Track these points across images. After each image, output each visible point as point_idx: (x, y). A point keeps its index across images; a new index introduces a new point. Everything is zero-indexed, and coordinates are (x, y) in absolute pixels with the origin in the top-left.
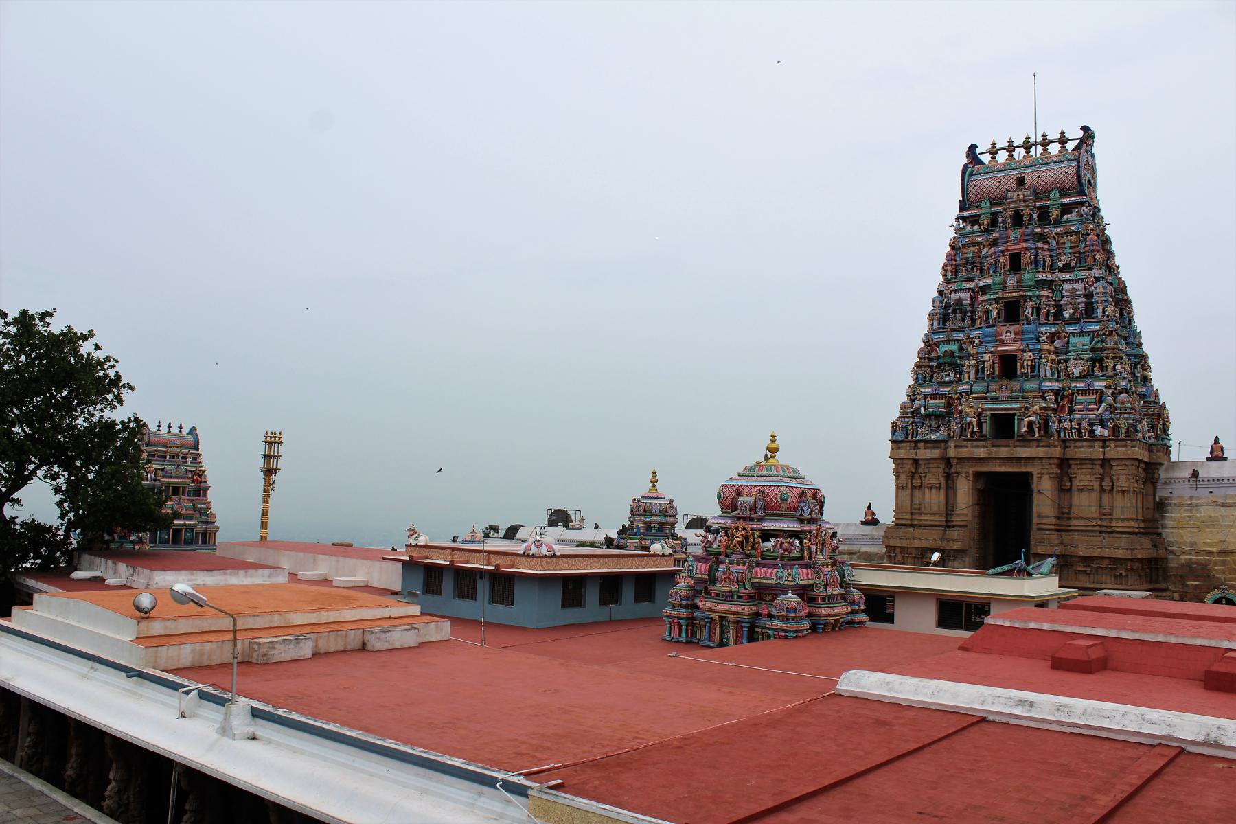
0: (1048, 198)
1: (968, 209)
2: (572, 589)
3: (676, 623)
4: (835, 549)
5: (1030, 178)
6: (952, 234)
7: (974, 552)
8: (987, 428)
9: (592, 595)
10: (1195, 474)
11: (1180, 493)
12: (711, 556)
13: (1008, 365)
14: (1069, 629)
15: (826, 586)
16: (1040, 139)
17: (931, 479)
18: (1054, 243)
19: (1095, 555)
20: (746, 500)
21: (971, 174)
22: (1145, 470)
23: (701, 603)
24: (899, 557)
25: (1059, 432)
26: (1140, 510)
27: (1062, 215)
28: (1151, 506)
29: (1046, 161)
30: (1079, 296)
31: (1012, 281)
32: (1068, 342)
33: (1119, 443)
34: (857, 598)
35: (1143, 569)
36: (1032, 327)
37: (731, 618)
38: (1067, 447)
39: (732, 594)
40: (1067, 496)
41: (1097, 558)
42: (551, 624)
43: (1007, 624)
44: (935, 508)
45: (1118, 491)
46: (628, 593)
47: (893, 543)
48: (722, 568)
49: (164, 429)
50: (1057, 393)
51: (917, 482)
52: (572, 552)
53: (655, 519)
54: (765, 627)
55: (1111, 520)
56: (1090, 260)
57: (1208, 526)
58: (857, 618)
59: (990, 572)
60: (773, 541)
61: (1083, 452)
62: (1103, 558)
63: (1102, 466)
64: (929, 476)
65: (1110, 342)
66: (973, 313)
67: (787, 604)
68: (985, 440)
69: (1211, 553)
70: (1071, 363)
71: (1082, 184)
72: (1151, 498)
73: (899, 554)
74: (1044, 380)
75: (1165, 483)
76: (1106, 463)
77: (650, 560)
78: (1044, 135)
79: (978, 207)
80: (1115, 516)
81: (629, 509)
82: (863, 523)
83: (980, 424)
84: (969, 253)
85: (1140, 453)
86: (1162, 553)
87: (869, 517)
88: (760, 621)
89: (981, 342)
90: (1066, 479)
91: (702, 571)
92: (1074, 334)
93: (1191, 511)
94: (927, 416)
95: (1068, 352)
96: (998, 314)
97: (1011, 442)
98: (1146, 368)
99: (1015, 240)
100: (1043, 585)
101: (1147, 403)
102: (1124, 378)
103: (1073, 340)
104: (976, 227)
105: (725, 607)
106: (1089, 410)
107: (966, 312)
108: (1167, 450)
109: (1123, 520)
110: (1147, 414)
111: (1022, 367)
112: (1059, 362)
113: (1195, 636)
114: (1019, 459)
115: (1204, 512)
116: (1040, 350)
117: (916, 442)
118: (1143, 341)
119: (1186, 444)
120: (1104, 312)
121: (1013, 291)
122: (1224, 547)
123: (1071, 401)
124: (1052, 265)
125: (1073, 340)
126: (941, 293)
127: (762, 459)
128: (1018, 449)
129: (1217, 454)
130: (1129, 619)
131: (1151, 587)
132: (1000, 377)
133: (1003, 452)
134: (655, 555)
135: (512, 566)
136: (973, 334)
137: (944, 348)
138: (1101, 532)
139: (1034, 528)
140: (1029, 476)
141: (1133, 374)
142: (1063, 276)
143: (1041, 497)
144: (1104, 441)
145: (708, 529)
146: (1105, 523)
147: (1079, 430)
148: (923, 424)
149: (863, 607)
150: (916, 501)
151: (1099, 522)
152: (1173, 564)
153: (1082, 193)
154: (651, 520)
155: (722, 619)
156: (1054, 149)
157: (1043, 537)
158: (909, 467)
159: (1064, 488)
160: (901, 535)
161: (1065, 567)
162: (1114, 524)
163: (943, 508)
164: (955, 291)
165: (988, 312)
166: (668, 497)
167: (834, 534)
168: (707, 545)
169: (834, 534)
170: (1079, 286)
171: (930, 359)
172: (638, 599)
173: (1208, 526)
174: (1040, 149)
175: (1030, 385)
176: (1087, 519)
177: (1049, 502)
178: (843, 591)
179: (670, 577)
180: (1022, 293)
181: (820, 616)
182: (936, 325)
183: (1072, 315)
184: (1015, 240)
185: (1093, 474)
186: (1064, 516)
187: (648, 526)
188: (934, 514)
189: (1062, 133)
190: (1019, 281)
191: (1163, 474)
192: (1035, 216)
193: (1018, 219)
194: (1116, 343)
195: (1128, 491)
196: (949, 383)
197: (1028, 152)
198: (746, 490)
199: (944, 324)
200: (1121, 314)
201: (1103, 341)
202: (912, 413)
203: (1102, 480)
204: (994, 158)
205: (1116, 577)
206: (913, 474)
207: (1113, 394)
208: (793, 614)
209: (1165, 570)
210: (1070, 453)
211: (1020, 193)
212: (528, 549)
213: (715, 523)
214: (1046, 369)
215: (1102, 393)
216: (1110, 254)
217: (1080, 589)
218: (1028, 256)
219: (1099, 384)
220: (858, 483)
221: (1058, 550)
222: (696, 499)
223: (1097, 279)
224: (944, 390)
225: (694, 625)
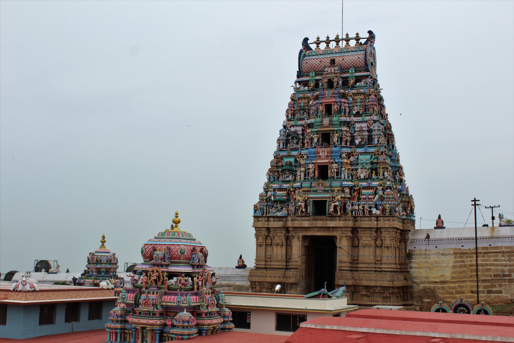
0: (348, 72)
1: (302, 76)
2: (46, 312)
3: (114, 332)
4: (214, 283)
5: (338, 60)
6: (293, 91)
7: (302, 284)
8: (310, 209)
9: (60, 316)
10: (428, 237)
11: (419, 248)
12: (137, 290)
13: (323, 172)
14: (348, 329)
15: (207, 307)
16: (344, 37)
17: (277, 240)
18: (351, 99)
19: (372, 285)
20: (159, 253)
21: (305, 56)
22: (401, 234)
23: (130, 319)
24: (258, 288)
25: (352, 212)
26: (397, 258)
27: (356, 82)
28: (404, 255)
29: (347, 50)
30: (364, 131)
31: (326, 121)
32: (358, 158)
33: (386, 218)
34: (227, 313)
35: (399, 293)
36: (337, 149)
37: (149, 328)
38: (356, 221)
39: (149, 313)
40: (356, 249)
41: (373, 287)
42: (32, 336)
43: (313, 327)
44: (280, 258)
45: (385, 247)
46: (84, 314)
48: (143, 296)
50: (351, 188)
51: (269, 241)
52: (47, 288)
53: (103, 266)
54: (169, 333)
55: (381, 264)
56: (371, 110)
57: (434, 267)
58: (227, 326)
59: (307, 296)
60: (175, 279)
61: (366, 223)
62: (376, 287)
63: (376, 232)
64: (276, 238)
65: (381, 158)
66: (303, 139)
67: (183, 318)
68: (309, 216)
69: (437, 282)
70: (359, 171)
71: (368, 65)
72: (404, 251)
73: (257, 287)
74: (344, 180)
75: (412, 242)
76: (378, 230)
77: (99, 292)
78: (347, 35)
79: (308, 76)
80: (383, 262)
81: (86, 260)
82: (237, 267)
83: (306, 207)
84: (302, 103)
85: (398, 224)
86: (410, 283)
87: (241, 263)
88: (167, 329)
89: (308, 157)
90: (356, 239)
91: (130, 298)
92: (361, 153)
93: (426, 258)
94: (275, 201)
95: (357, 164)
96: (318, 140)
97: (324, 217)
98: (402, 174)
99: (329, 96)
100: (338, 302)
101: (402, 195)
102: (389, 180)
103: (361, 157)
104: (306, 88)
105: (145, 321)
106: (369, 199)
107: (299, 139)
108: (413, 222)
109: (388, 264)
110: (402, 202)
111: (331, 173)
112: (352, 170)
113: (415, 330)
114: (329, 228)
115: (433, 258)
116: (342, 163)
117: (268, 217)
118: (400, 158)
119: (423, 220)
120: (378, 141)
121: (327, 127)
122: (443, 279)
123: (359, 193)
124: (349, 112)
125: (361, 157)
126: (285, 127)
127: (169, 228)
128: (328, 222)
129: (440, 225)
130: (382, 322)
131: (403, 303)
132: (318, 178)
133: (320, 224)
134: (103, 289)
135: (6, 299)
136: (303, 152)
137: (286, 160)
138: (375, 271)
139: (337, 269)
140: (335, 238)
141: (394, 178)
142: (356, 119)
143: (342, 251)
144: (377, 217)
145: (135, 272)
146: (378, 266)
147: (363, 211)
148: (273, 206)
149: (231, 319)
150: (268, 253)
151: (374, 265)
152: (416, 289)
153: (367, 70)
154: (101, 267)
155: (143, 328)
156: (353, 43)
157: (343, 276)
158: (264, 232)
159: (355, 246)
160: (259, 274)
161: (353, 292)
162: (383, 266)
163: (284, 258)
164: (293, 126)
165: (312, 139)
166: (112, 252)
167: (213, 274)
168: (134, 282)
169: (213, 274)
170: (364, 125)
171: (277, 167)
172: (91, 318)
173: (434, 267)
174: (345, 43)
175: (336, 184)
176: (368, 263)
177: (346, 254)
178: (218, 309)
179: (112, 303)
180: (332, 129)
181: (204, 325)
182: (281, 146)
183: (360, 142)
184: (329, 96)
185: (371, 237)
186: (354, 261)
187: (99, 271)
188: (279, 261)
189: (357, 34)
190: (331, 121)
191: (410, 236)
192: (340, 83)
193: (330, 84)
194: (384, 159)
195: (391, 247)
196: (289, 182)
197: (337, 44)
198: (159, 247)
199: (286, 146)
200: (388, 143)
201: (377, 158)
202: (266, 199)
203: (376, 240)
204: (318, 47)
205: (384, 297)
206: (267, 237)
207: (383, 189)
208: (186, 324)
209: (412, 294)
210: (358, 224)
211: (332, 69)
212: (17, 287)
213: (139, 268)
214: (345, 174)
215: (376, 189)
216: (382, 107)
217: (360, 305)
218: (336, 106)
219: (375, 184)
220: (231, 243)
221: (350, 283)
222: (129, 255)
223: (375, 121)
224: (285, 186)
225: (125, 333)
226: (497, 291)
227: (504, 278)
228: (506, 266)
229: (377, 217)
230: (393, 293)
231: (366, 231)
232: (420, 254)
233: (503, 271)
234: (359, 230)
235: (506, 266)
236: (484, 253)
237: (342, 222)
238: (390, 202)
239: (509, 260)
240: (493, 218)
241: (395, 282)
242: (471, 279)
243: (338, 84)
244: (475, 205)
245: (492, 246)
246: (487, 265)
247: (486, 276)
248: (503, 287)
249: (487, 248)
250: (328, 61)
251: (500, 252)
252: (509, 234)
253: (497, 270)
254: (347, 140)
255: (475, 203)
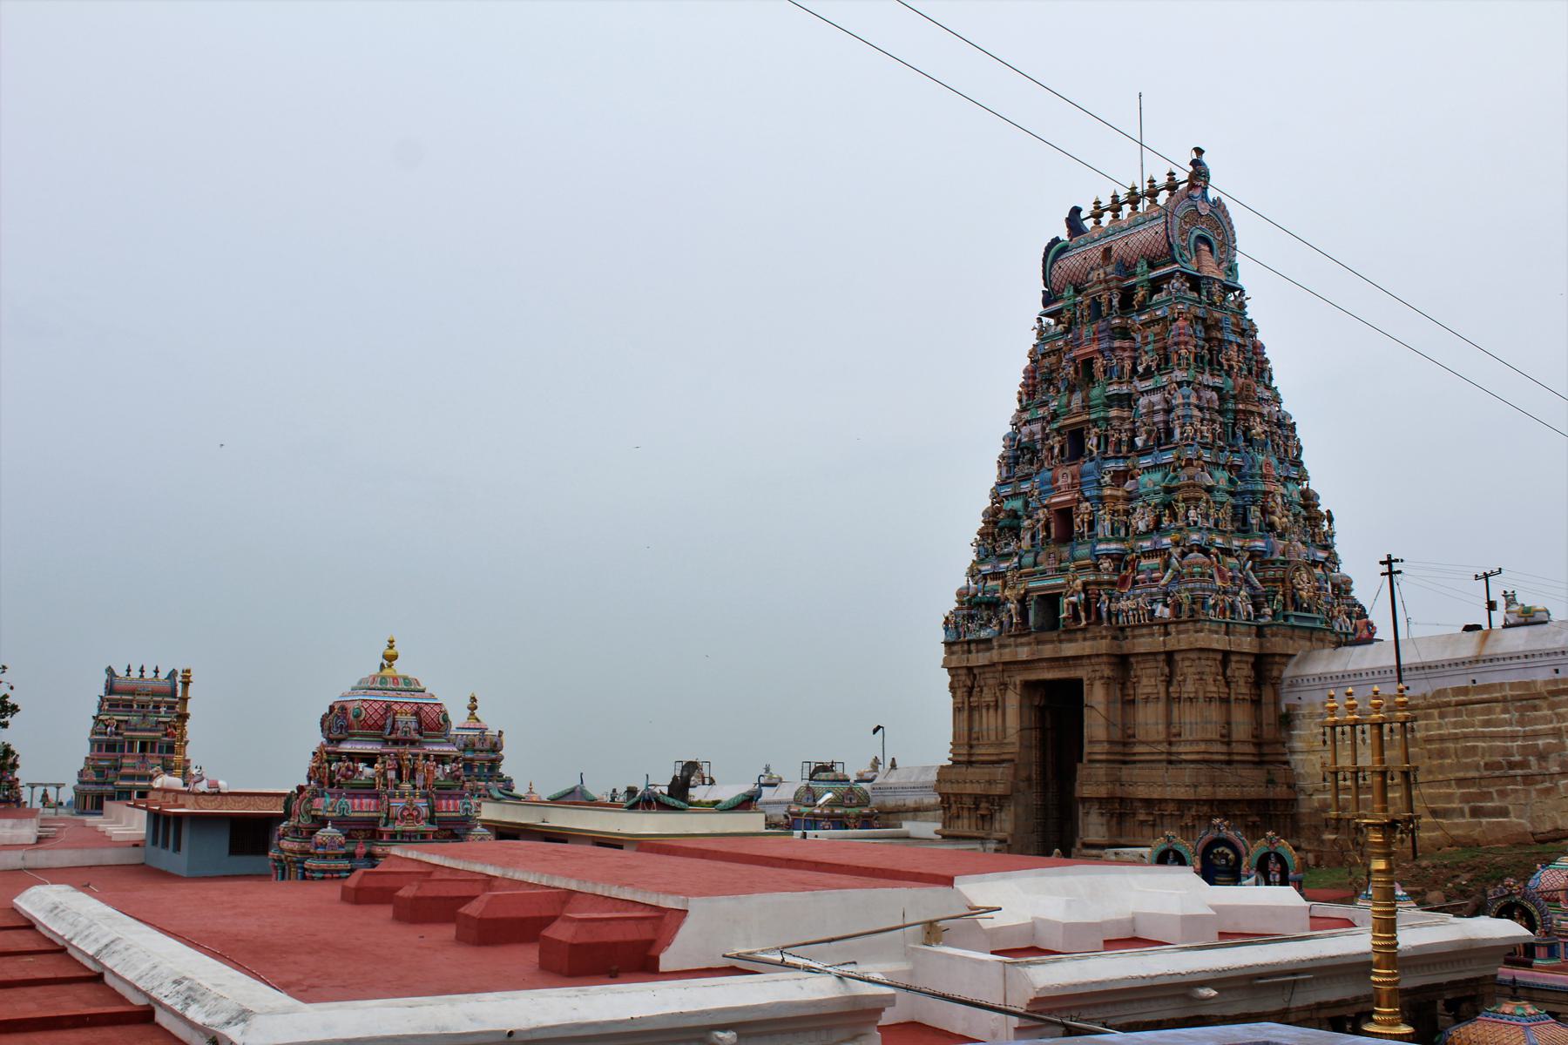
5: (1118, 248)
6: (1032, 339)
16: (1146, 187)
19: (1155, 796)
28: (1272, 720)
30: (1157, 412)
33: (1182, 627)
47: (948, 789)
49: (135, 674)
72: (1272, 708)
74: (1100, 541)
75: (1291, 685)
97: (1054, 634)
114: (1066, 659)
117: (969, 642)
121: (1078, 414)
128: (1065, 646)
143: (1094, 713)
170: (1156, 398)
183: (1146, 441)
188: (991, 745)
192: (1115, 302)
209: (1294, 819)
210: (1127, 647)
214: (1104, 528)
226: (1494, 808)
227: (1512, 772)
228: (1514, 737)
229: (1166, 625)
230: (1199, 817)
231: (1145, 661)
232: (1311, 716)
233: (1507, 752)
234: (1132, 660)
235: (1514, 737)
236: (1458, 704)
237: (1088, 643)
238: (1190, 585)
239: (1521, 723)
240: (1491, 606)
241: (1200, 789)
242: (1431, 778)
243: (1111, 306)
244: (1391, 573)
245: (1479, 683)
246: (1466, 737)
247: (1467, 767)
248: (1510, 798)
249: (1465, 691)
250: (1099, 254)
251: (1496, 701)
252: (1521, 648)
253: (1491, 750)
254: (1120, 440)
255: (1390, 567)
